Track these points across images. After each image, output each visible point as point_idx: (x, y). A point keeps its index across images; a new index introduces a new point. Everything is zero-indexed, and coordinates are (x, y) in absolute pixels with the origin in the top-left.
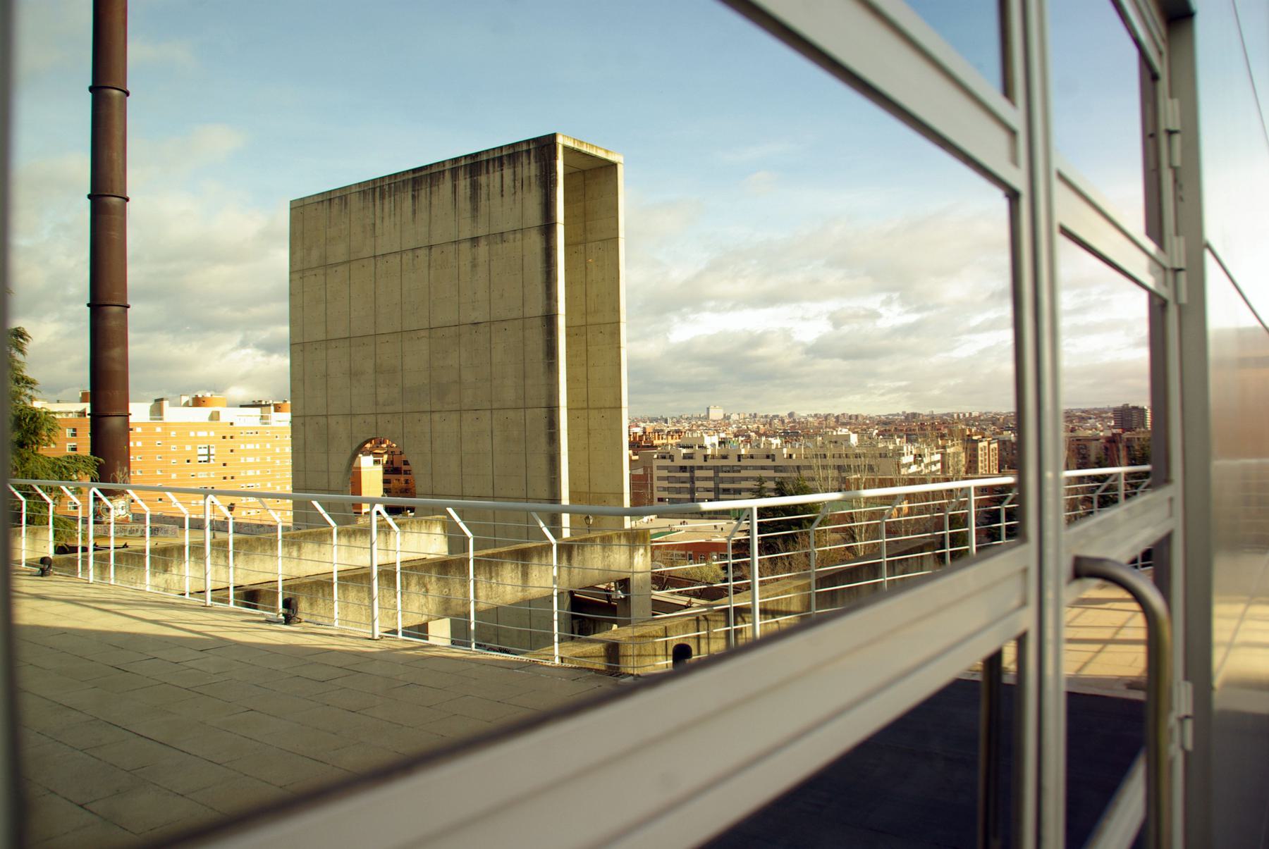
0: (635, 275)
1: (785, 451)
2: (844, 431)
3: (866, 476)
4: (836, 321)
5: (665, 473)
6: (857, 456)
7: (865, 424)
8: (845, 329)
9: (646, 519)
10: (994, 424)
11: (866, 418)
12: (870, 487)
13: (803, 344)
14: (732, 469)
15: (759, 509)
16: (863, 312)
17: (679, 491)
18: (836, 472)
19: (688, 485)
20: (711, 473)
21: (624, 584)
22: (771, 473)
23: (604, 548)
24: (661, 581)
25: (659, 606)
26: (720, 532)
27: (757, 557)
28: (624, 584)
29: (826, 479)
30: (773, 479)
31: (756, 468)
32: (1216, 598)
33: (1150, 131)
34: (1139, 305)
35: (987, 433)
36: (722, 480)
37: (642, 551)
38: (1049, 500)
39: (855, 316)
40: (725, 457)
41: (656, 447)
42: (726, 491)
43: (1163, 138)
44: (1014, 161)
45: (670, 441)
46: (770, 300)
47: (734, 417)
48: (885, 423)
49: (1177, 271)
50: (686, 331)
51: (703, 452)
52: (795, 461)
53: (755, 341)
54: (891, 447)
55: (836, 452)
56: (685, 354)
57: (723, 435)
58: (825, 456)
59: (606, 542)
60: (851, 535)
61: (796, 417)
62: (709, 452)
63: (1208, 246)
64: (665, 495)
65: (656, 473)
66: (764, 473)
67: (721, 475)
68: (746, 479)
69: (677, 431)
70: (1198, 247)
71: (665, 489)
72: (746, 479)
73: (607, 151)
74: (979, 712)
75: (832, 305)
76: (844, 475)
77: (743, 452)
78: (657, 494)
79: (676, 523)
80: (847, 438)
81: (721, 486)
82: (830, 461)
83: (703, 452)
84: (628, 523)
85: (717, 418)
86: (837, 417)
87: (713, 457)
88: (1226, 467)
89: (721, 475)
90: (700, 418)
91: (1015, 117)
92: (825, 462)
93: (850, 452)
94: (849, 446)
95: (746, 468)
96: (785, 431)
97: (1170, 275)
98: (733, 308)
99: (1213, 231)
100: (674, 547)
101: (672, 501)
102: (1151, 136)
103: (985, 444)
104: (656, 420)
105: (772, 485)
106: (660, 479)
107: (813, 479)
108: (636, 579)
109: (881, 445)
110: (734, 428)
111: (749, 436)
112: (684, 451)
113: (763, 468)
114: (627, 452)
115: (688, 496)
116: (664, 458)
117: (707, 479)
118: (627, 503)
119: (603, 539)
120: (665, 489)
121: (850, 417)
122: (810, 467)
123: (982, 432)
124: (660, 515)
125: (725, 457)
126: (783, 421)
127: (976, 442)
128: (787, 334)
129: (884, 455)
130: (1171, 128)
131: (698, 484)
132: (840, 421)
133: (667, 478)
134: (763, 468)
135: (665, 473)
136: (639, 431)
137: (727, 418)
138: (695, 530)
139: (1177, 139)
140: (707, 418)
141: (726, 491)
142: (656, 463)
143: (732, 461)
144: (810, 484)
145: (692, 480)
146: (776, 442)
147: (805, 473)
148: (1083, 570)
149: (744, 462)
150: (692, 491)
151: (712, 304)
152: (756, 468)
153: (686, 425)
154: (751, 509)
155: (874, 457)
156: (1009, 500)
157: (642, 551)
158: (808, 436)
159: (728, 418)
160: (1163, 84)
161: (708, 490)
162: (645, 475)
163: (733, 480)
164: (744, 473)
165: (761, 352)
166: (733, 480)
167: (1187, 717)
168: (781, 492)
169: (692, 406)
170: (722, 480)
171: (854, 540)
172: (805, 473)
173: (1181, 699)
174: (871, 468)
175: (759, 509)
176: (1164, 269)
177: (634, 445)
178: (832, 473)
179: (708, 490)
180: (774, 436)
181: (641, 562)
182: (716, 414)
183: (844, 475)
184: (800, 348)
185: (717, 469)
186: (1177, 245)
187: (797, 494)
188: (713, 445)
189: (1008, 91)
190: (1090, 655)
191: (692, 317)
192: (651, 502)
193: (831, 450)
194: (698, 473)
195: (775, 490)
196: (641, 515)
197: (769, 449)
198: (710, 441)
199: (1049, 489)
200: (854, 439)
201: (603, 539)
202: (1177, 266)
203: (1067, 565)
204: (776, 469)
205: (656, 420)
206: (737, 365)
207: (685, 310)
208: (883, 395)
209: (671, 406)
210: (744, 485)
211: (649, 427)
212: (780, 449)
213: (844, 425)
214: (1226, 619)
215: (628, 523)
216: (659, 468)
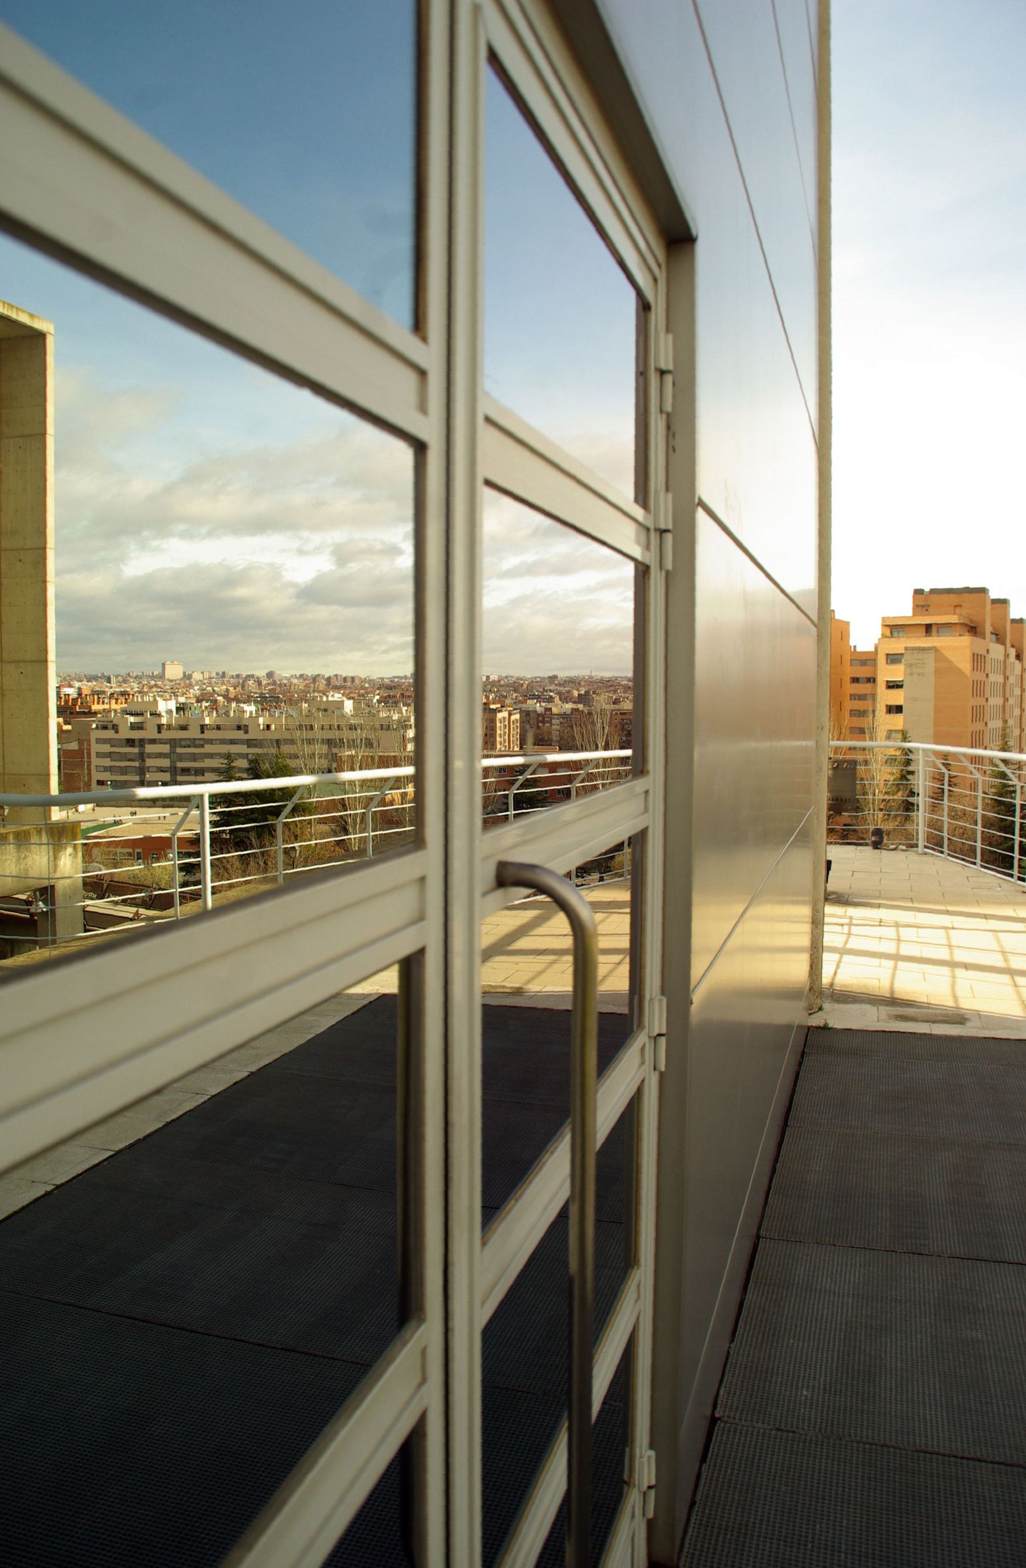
0: (67, 486)
1: (261, 720)
2: (337, 697)
3: (361, 753)
4: (342, 555)
5: (106, 748)
6: (352, 728)
7: (363, 688)
8: (353, 567)
9: (81, 808)
10: (515, 691)
11: (364, 681)
12: (368, 767)
13: (294, 585)
14: (193, 743)
15: (211, 796)
16: (379, 547)
17: (124, 771)
18: (325, 749)
19: (137, 764)
20: (166, 749)
21: (47, 892)
22: (243, 749)
23: (19, 846)
24: (96, 887)
25: (92, 920)
26: (159, 823)
27: (209, 858)
28: (47, 892)
29: (312, 756)
30: (245, 756)
31: (223, 742)
32: (696, 898)
33: (641, 369)
34: (630, 569)
35: (508, 701)
36: (181, 758)
37: (70, 850)
38: (459, 798)
39: (370, 551)
40: (184, 728)
41: (95, 713)
42: (186, 771)
43: (654, 379)
44: (423, 408)
45: (114, 706)
46: (260, 525)
47: (197, 676)
48: (389, 688)
49: (663, 532)
50: (151, 561)
51: (156, 721)
52: (273, 734)
53: (233, 579)
54: (396, 717)
55: (326, 723)
56: (143, 592)
57: (182, 700)
58: (312, 728)
59: (22, 839)
60: (342, 826)
61: (276, 678)
62: (164, 721)
63: (701, 504)
64: (106, 776)
65: (95, 748)
66: (234, 749)
67: (179, 750)
68: (211, 756)
69: (124, 694)
70: (688, 504)
71: (106, 769)
72: (211, 756)
73: (32, 316)
74: (379, 1041)
75: (337, 536)
76: (335, 750)
77: (207, 721)
78: (96, 776)
79: (123, 813)
80: (340, 705)
81: (180, 765)
82: (317, 734)
83: (156, 721)
84: (57, 814)
85: (177, 678)
86: (329, 679)
87: (169, 727)
88: (713, 754)
89: (179, 750)
90: (153, 677)
91: (429, 355)
92: (310, 735)
93: (343, 723)
94: (343, 716)
95: (211, 742)
96: (262, 696)
97: (654, 537)
98: (210, 534)
99: (706, 488)
100: (117, 844)
101: (116, 784)
102: (641, 374)
103: (505, 714)
104: (95, 678)
105: (243, 763)
106: (100, 755)
107: (296, 757)
108: (61, 886)
109: (383, 714)
110: (196, 691)
111: (216, 701)
112: (132, 719)
113: (232, 742)
114: (54, 721)
115: (137, 778)
116: (105, 728)
117: (160, 755)
118: (54, 789)
119: (18, 835)
120: (106, 769)
121: (345, 679)
122: (292, 742)
123: (501, 699)
124: (100, 803)
125: (184, 728)
126: (259, 683)
127: (495, 711)
128: (275, 572)
129: (386, 727)
130: (663, 367)
131: (149, 762)
132: (331, 684)
133: (109, 755)
134: (232, 742)
135: (106, 748)
136: (72, 692)
137: (187, 677)
138: (145, 822)
139: (669, 379)
140: (162, 676)
141: (186, 771)
142: (95, 735)
143: (193, 733)
144: (292, 763)
145: (142, 757)
146: (250, 709)
147: (286, 749)
148: (509, 877)
149: (208, 735)
150: (142, 771)
151: (182, 527)
152: (223, 742)
153: (136, 687)
154: (202, 796)
155: (373, 728)
156: (518, 784)
157: (70, 850)
158: (291, 702)
159: (190, 677)
160: (658, 315)
161: (162, 770)
162: (80, 753)
163: (194, 757)
164: (209, 749)
165: (241, 592)
166: (194, 757)
167: (659, 1035)
168: (257, 775)
169: (145, 661)
170: (181, 758)
171: (347, 833)
172: (286, 749)
173: (656, 1016)
174: (369, 744)
175: (211, 796)
176: (648, 530)
177: (66, 710)
178: (321, 749)
179: (162, 770)
180: (247, 701)
181: (69, 866)
182: (174, 672)
183: (335, 750)
184: (291, 591)
185: (174, 743)
186: (664, 503)
187: (275, 775)
188: (169, 712)
189: (419, 325)
190: (544, 966)
191: (154, 543)
192: (88, 786)
193: (320, 720)
194: (149, 748)
195: (248, 770)
196: (74, 804)
197: (241, 718)
198: (166, 706)
199: (459, 783)
200: (349, 706)
201: (18, 835)
202: (663, 527)
203: (487, 872)
204: (250, 743)
205: (95, 678)
206: (208, 608)
207: (145, 533)
208: (386, 652)
209: (115, 660)
210: (208, 763)
211: (87, 687)
212: (254, 719)
213: (337, 688)
214: (709, 923)
215: (57, 814)
216: (99, 741)
